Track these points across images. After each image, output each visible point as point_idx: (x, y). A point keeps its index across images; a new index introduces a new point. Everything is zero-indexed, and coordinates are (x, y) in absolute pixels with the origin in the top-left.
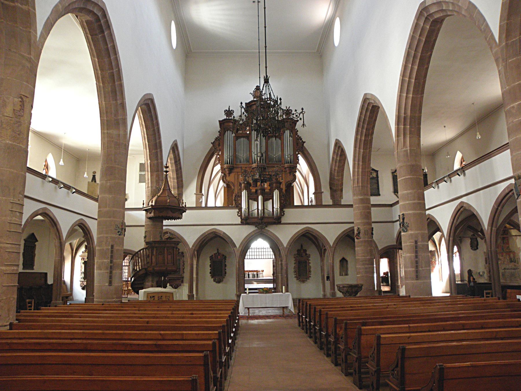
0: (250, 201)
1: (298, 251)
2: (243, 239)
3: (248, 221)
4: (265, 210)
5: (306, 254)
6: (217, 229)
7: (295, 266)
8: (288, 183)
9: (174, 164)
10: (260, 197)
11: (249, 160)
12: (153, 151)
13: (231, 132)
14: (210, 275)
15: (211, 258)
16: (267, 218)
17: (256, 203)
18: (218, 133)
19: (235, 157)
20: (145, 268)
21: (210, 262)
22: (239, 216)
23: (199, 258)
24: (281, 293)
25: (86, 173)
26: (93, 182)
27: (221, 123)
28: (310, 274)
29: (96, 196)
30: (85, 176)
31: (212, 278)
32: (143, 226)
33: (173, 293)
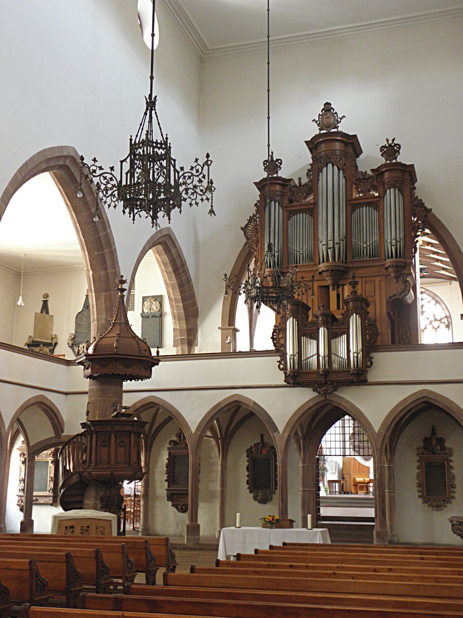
0: (303, 339)
1: (425, 440)
2: (292, 414)
3: (299, 380)
4: (333, 356)
5: (443, 448)
6: (242, 396)
7: (418, 474)
8: (393, 298)
9: (173, 274)
10: (322, 331)
11: (312, 257)
12: (96, 253)
13: (277, 204)
14: (248, 486)
15: (249, 452)
16: (337, 372)
17: (315, 342)
18: (255, 208)
19: (286, 251)
20: (79, 472)
21: (248, 461)
22: (281, 370)
23: (227, 451)
24: (233, 528)
25: (21, 298)
26: (44, 313)
27: (260, 185)
28: (454, 492)
29: (48, 339)
30: (19, 303)
31: (251, 492)
32: (86, 393)
33: (111, 521)
